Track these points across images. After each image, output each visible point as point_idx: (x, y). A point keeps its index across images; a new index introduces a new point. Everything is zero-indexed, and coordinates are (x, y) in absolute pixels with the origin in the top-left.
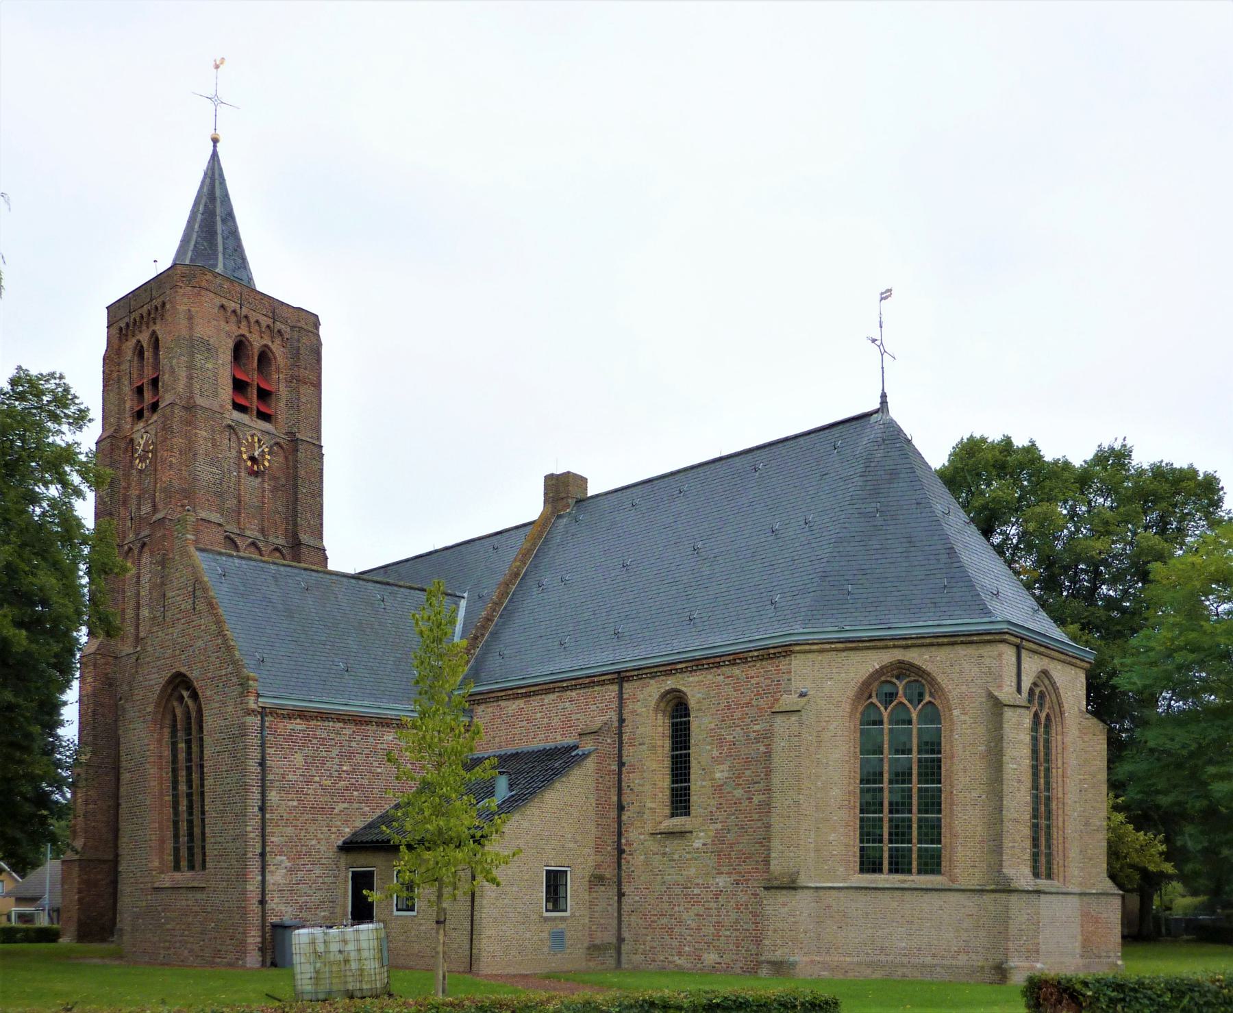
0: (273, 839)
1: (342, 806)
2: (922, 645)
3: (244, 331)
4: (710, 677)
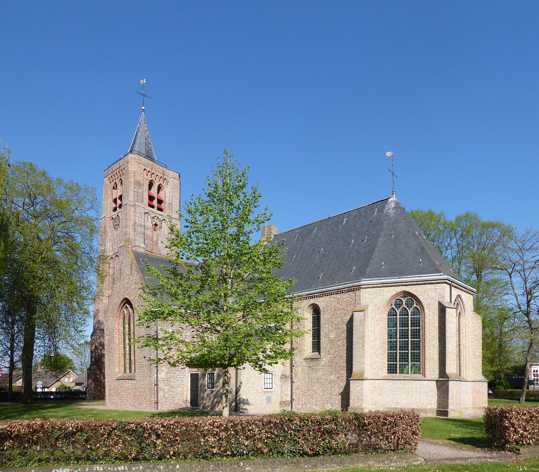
2: (413, 285)
3: (153, 178)
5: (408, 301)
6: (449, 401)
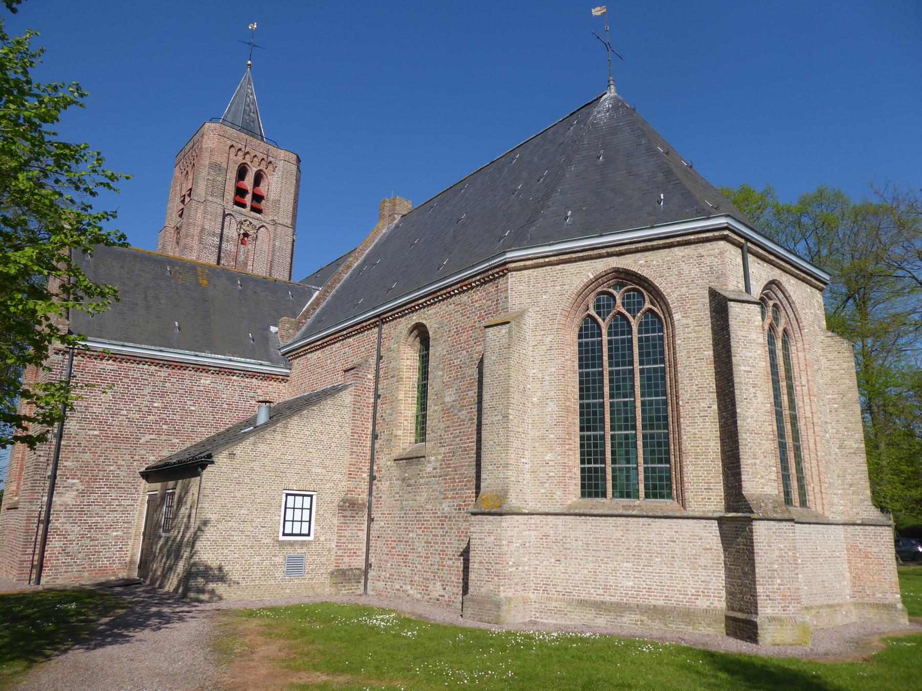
0: (66, 464)
1: (148, 437)
3: (248, 160)
4: (444, 307)
5: (629, 297)
6: (760, 589)
